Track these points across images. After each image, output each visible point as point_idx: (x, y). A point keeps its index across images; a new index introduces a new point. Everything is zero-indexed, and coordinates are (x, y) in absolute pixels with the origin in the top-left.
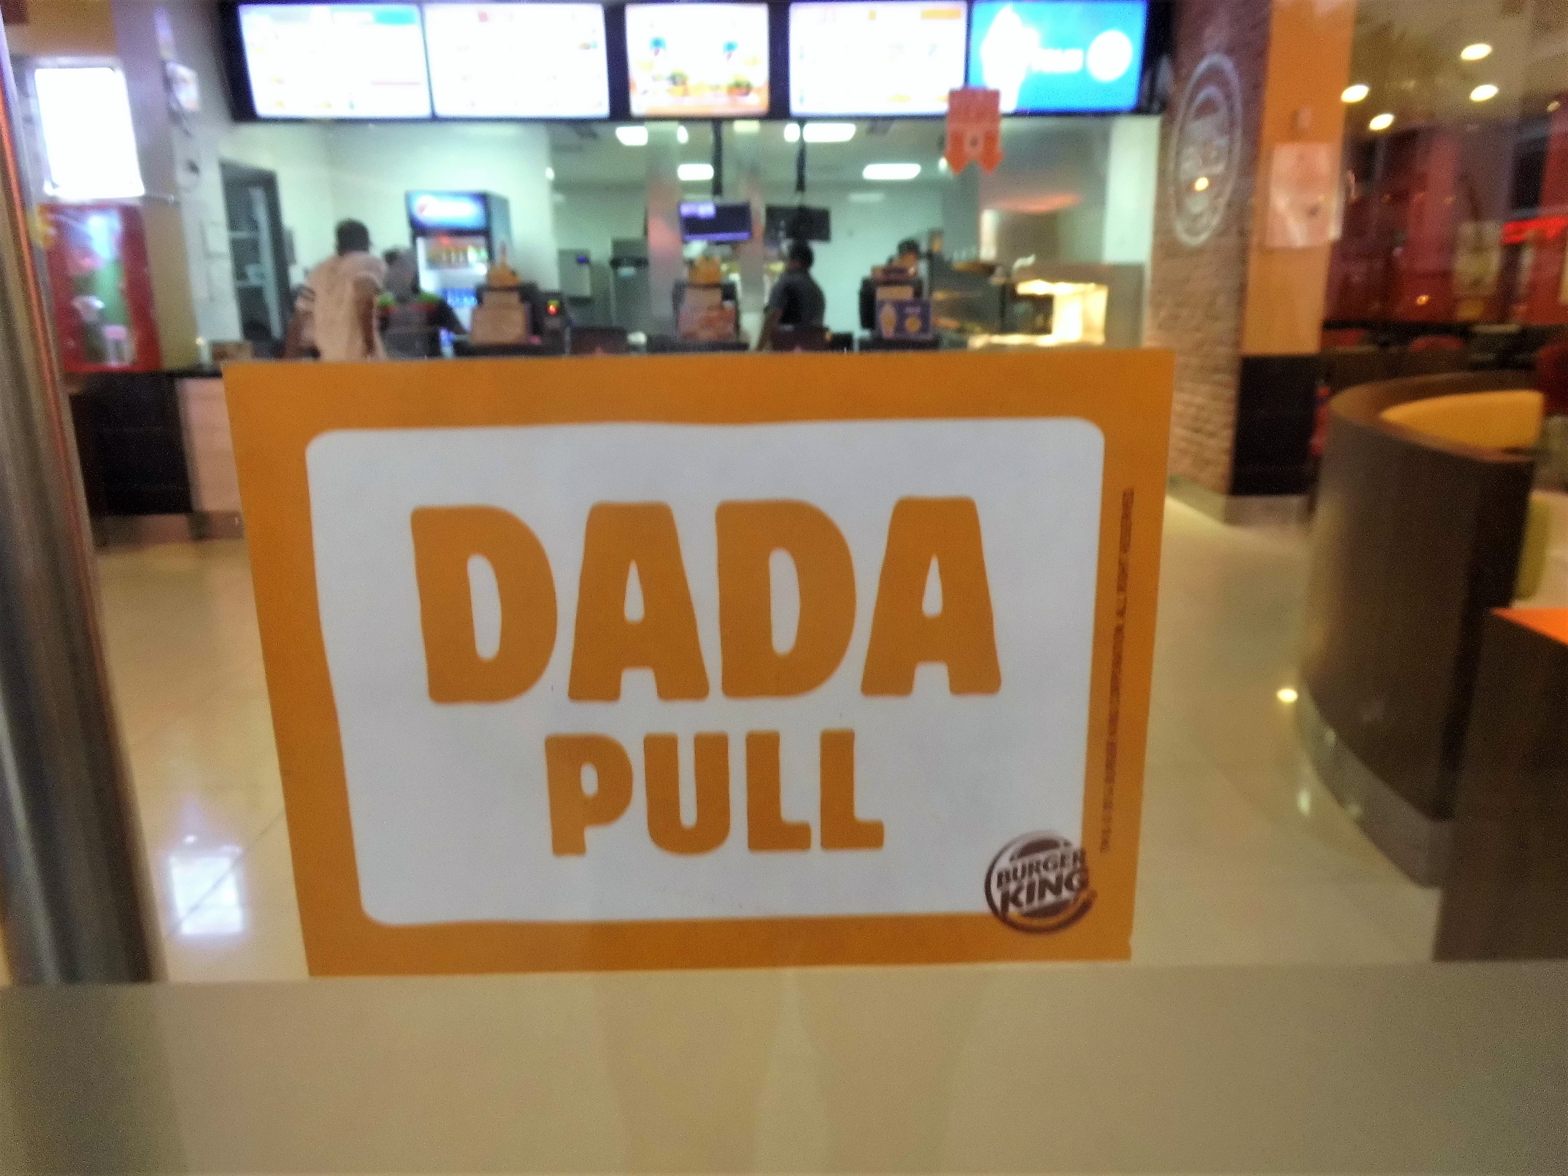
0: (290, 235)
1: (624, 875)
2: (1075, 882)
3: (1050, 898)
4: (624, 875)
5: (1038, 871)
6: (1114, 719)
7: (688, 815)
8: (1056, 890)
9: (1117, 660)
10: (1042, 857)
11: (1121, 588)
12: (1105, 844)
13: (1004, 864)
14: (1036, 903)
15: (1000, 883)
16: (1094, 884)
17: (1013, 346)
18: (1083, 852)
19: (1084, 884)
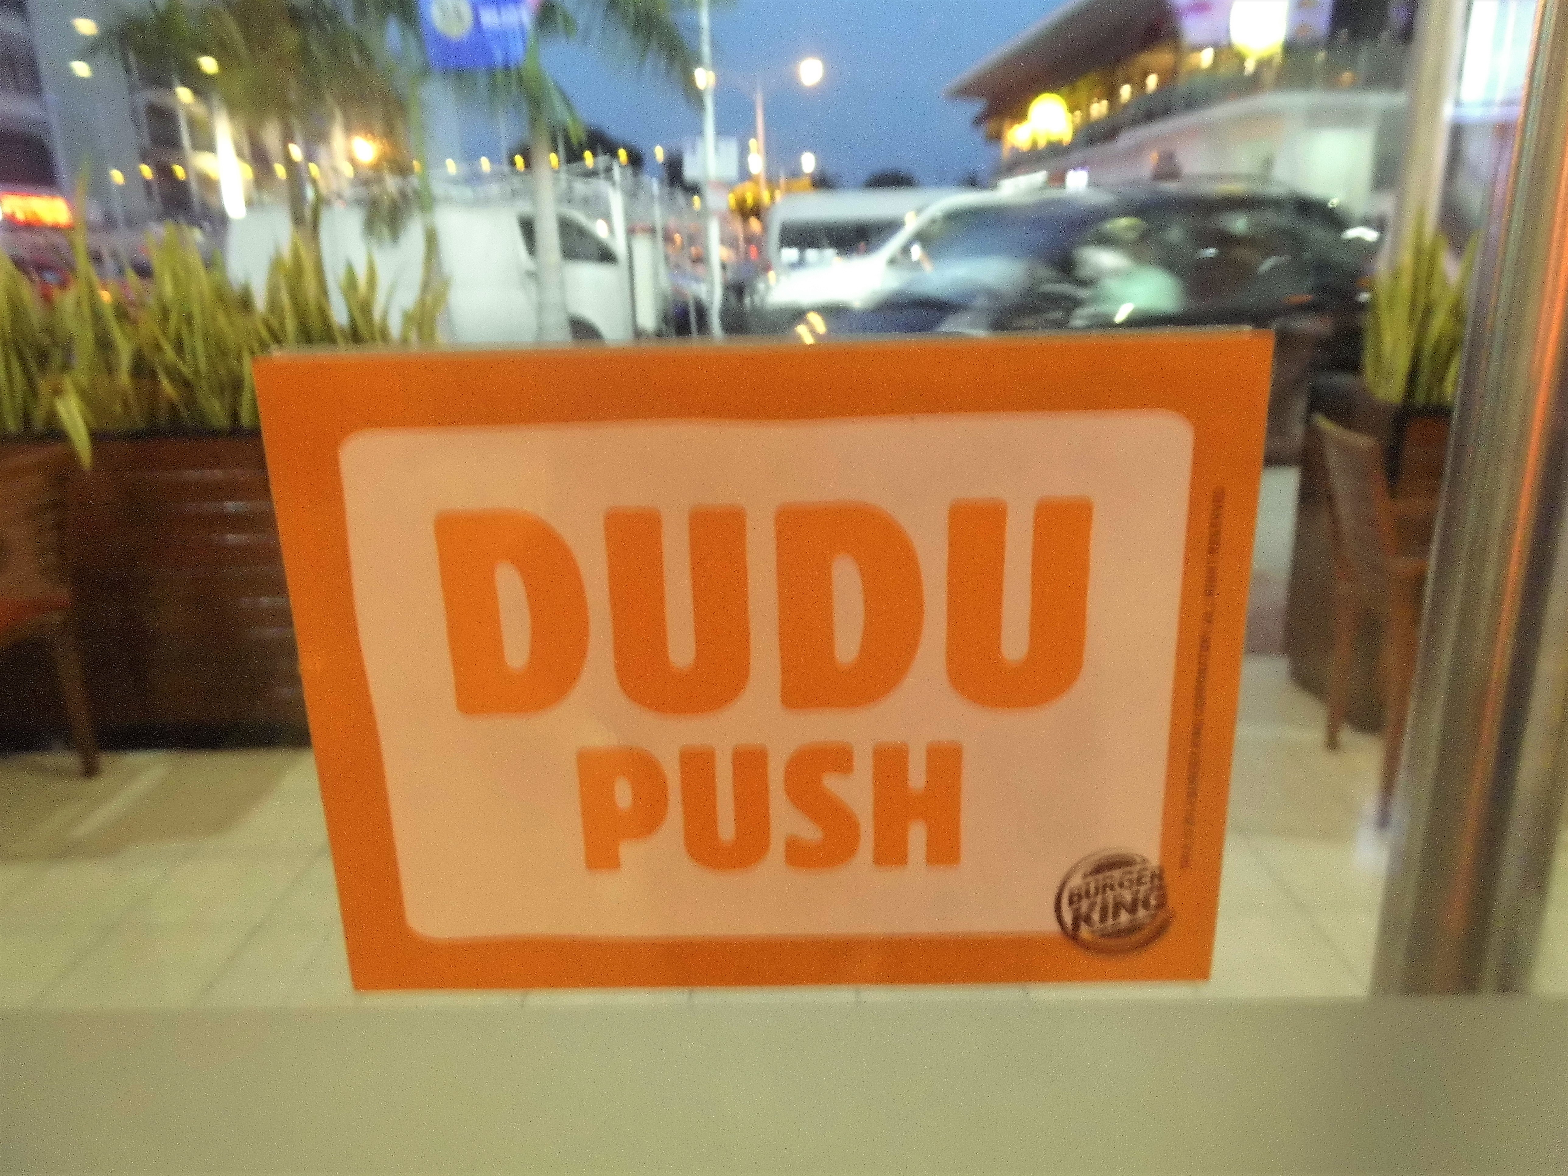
0: (240, 154)
1: (651, 891)
2: (1153, 902)
3: (1124, 917)
4: (651, 891)
5: (1112, 889)
6: (1197, 731)
7: (727, 829)
8: (1132, 910)
9: (1202, 672)
10: (1116, 874)
11: (1209, 592)
12: (1185, 861)
13: (1076, 881)
14: (1110, 921)
15: (1071, 902)
16: (1173, 902)
17: (1068, 104)
18: (1162, 869)
19: (1161, 905)
